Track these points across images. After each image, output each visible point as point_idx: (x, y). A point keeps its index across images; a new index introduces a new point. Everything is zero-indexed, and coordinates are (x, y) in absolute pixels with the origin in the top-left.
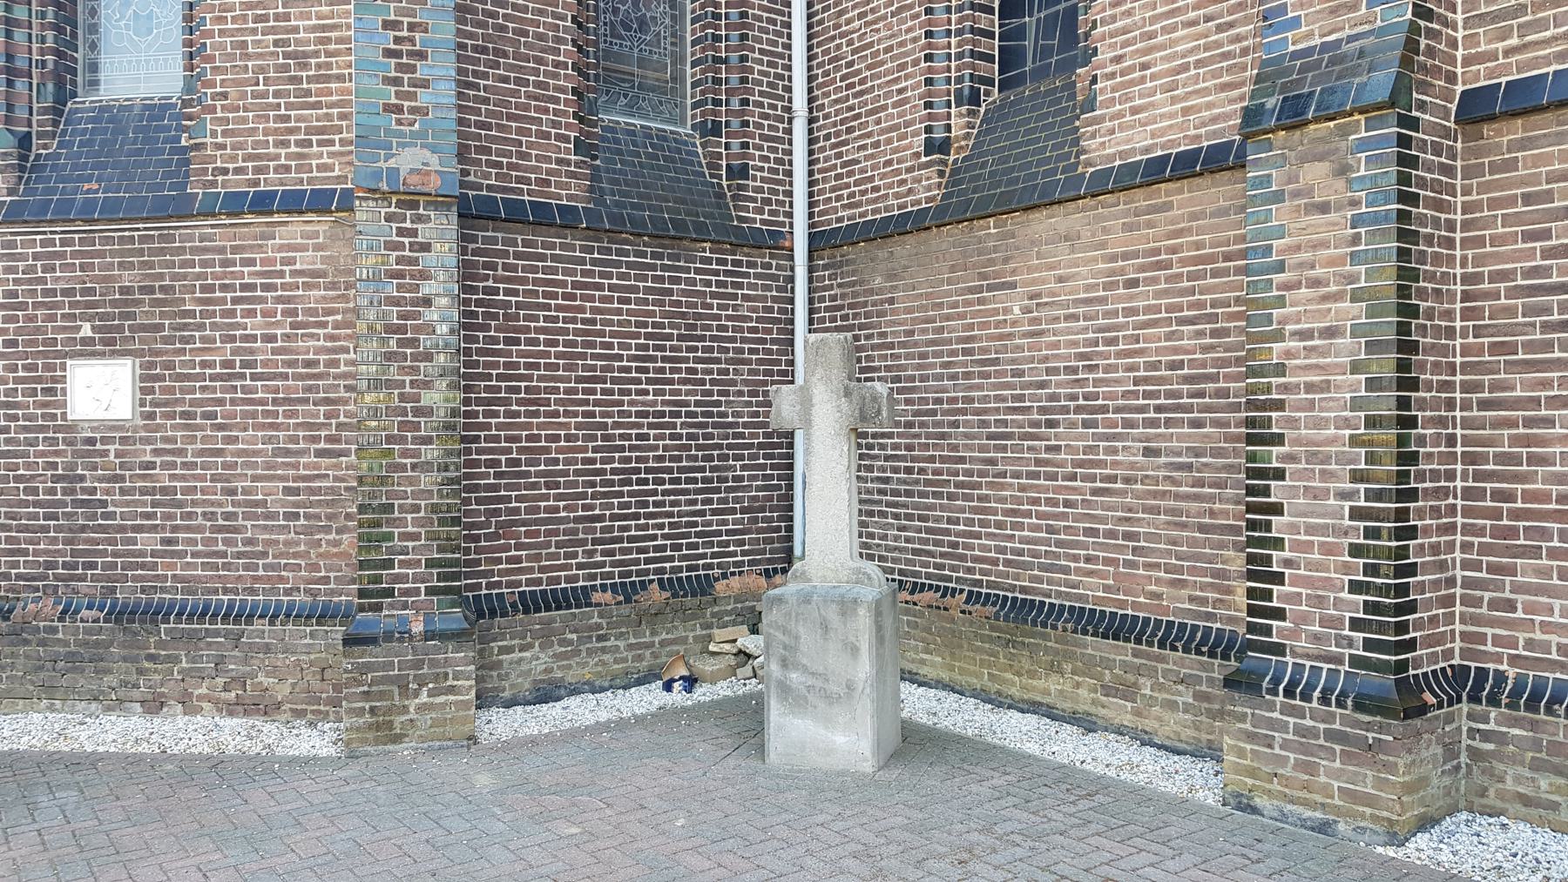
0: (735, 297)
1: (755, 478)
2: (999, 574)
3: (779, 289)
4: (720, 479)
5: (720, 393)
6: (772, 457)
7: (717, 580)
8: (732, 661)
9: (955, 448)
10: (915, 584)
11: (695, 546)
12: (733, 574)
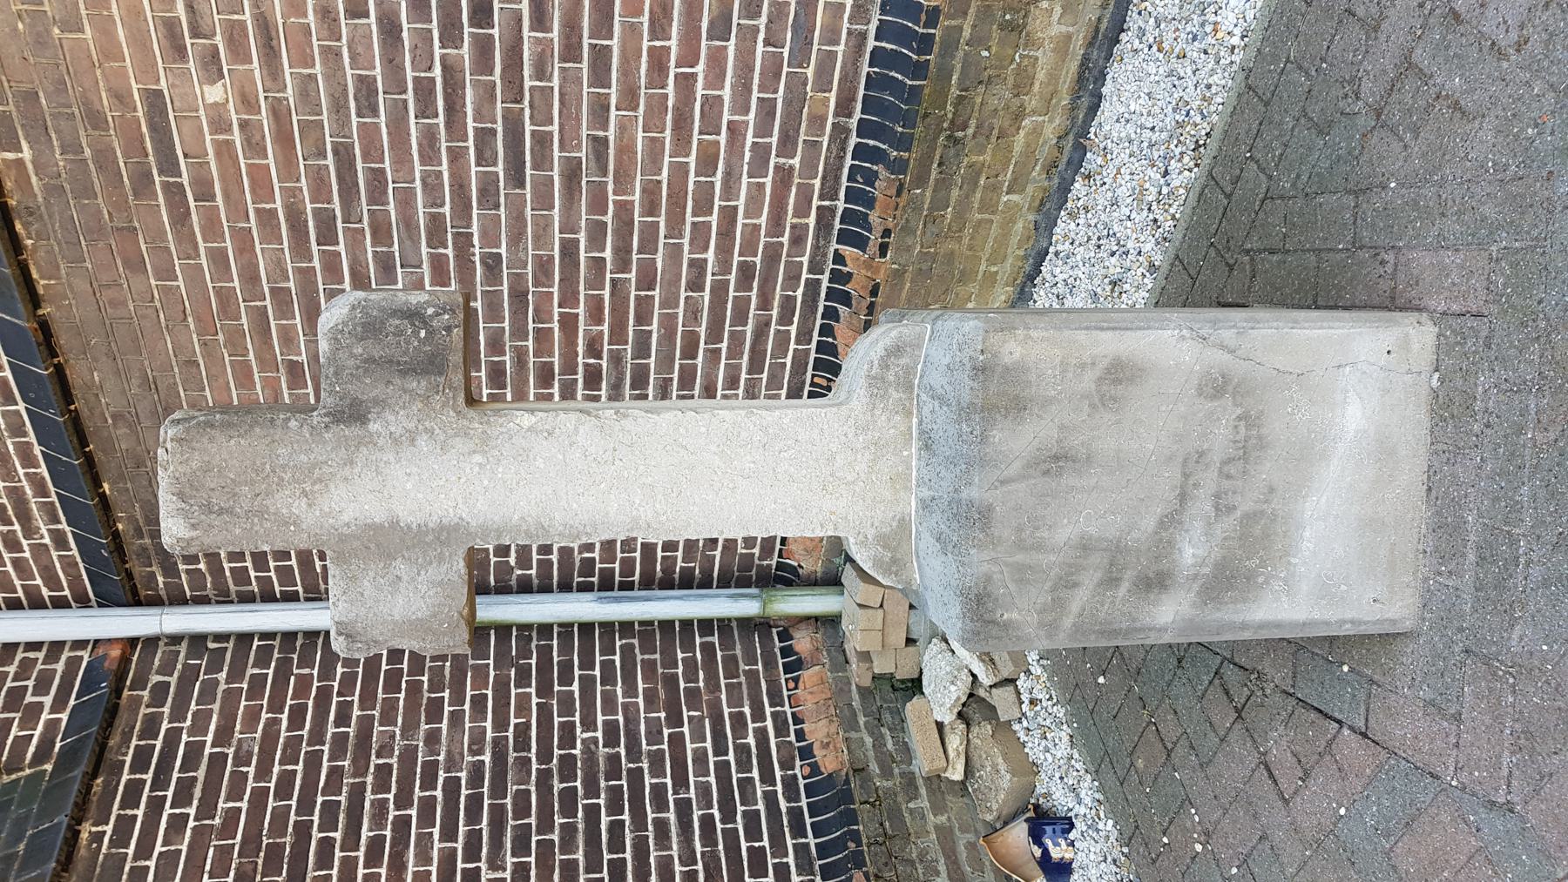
0: (218, 761)
1: (609, 700)
2: (809, 166)
3: (215, 667)
4: (614, 771)
5: (429, 783)
6: (566, 669)
7: (815, 769)
8: (984, 730)
9: (543, 266)
10: (818, 365)
11: (752, 819)
12: (800, 735)
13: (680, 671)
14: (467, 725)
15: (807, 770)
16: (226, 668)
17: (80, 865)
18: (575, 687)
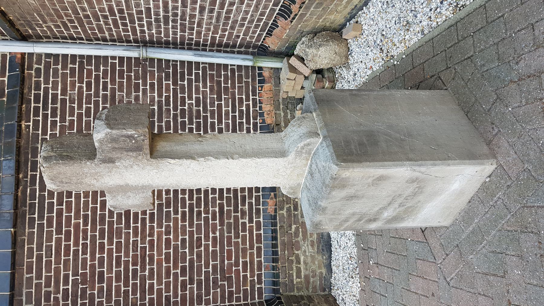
0: (63, 101)
13: (222, 79)
14: (149, 95)
15: (261, 121)
16: (60, 64)
17: (24, 137)
18: (186, 83)
